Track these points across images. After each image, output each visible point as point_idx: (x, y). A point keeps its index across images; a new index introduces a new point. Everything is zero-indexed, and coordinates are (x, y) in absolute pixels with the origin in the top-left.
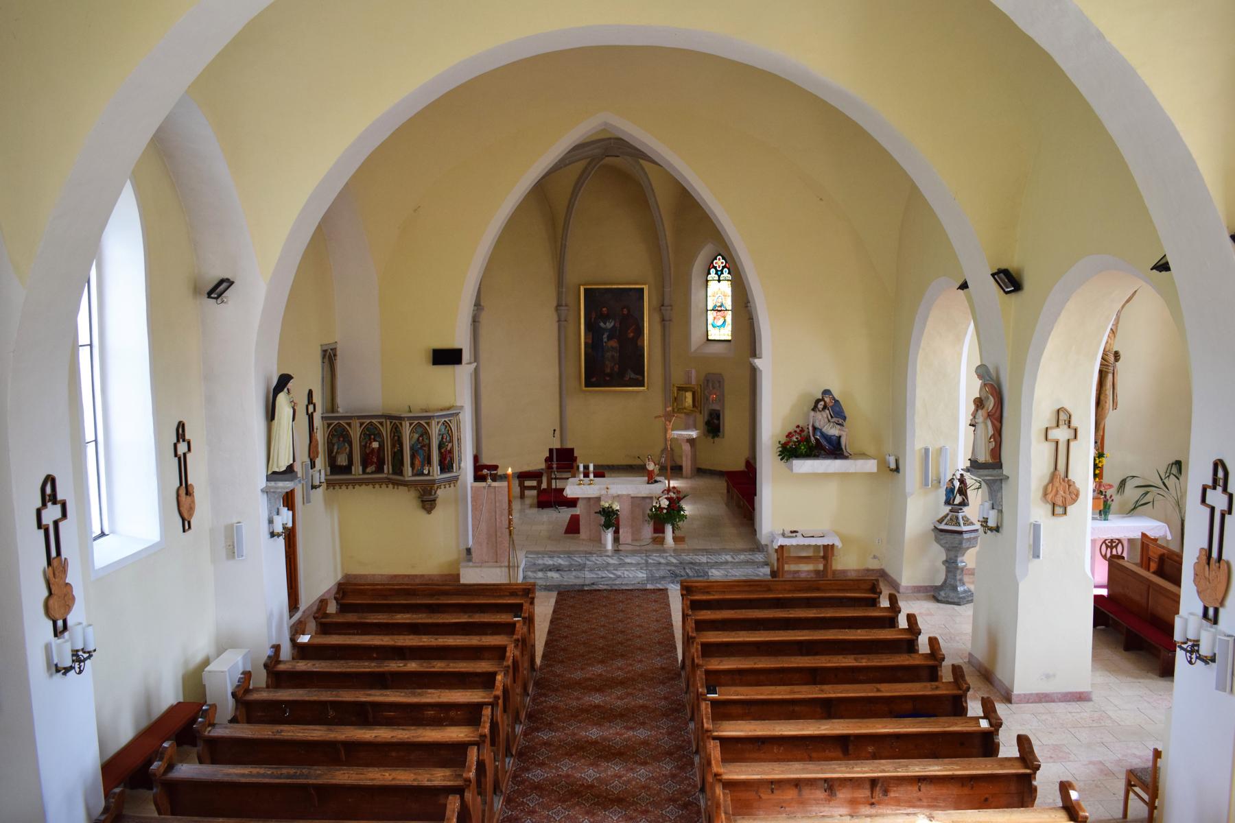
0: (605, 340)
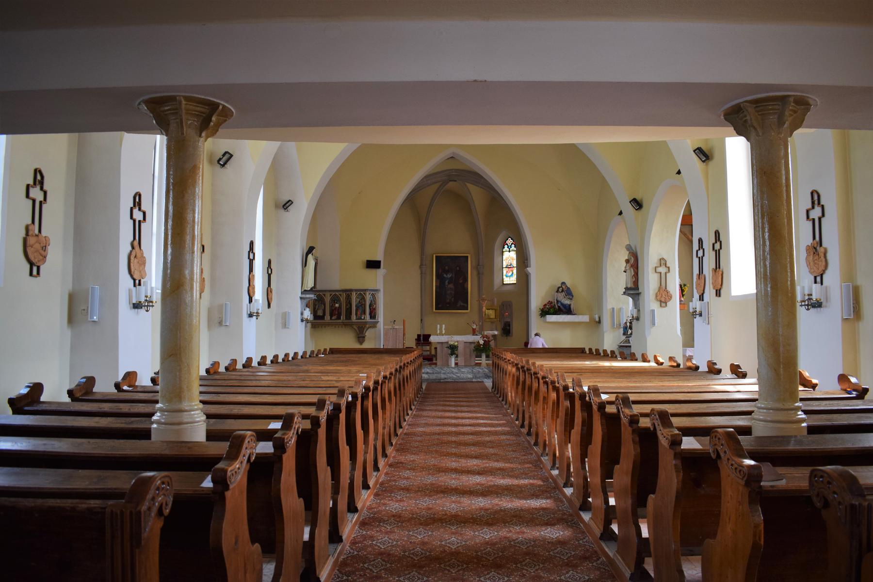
0: (447, 284)
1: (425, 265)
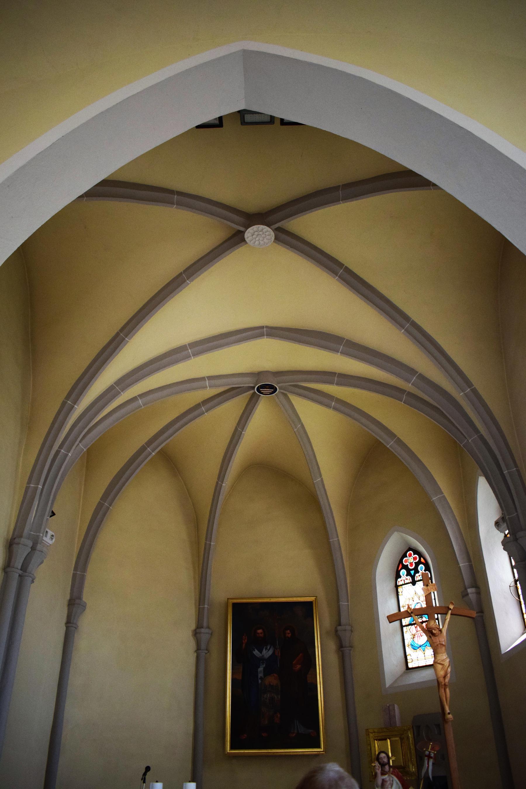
0: (260, 675)
1: (208, 627)
